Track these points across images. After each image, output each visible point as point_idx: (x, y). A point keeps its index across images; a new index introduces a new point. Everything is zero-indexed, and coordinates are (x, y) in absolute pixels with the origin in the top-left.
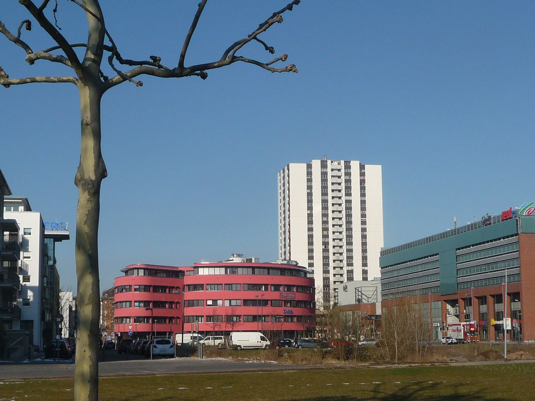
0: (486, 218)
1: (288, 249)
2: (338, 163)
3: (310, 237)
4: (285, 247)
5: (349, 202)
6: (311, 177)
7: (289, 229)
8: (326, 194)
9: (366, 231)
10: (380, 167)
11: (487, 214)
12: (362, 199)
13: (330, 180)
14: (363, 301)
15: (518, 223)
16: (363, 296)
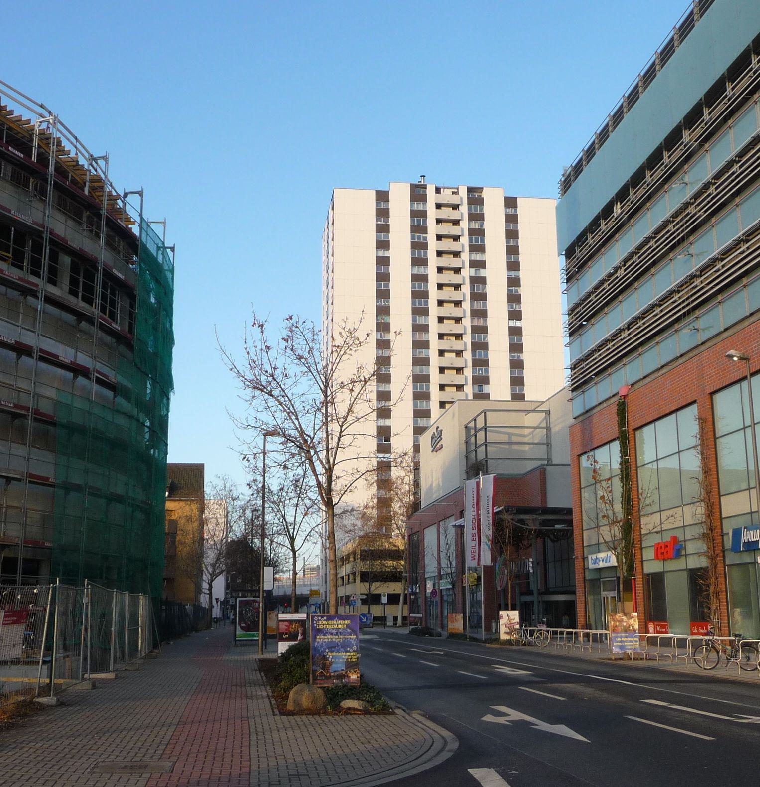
5: (478, 281)
8: (425, 312)
9: (522, 351)
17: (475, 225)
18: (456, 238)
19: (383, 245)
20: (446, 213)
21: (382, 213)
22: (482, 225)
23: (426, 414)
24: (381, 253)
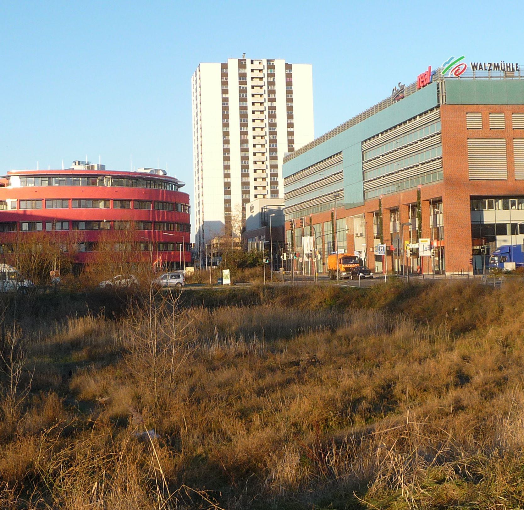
0: (398, 89)
3: (226, 151)
6: (226, 79)
10: (310, 66)
11: (399, 84)
15: (440, 89)
19: (226, 142)
21: (224, 75)
22: (274, 80)
23: (248, 201)
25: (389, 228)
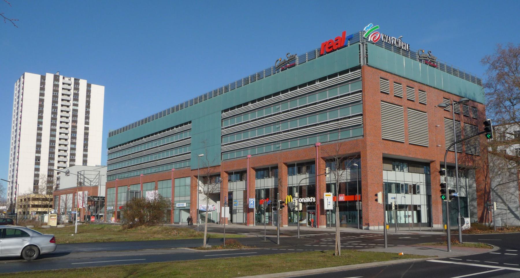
1: (18, 143)
2: (69, 79)
3: (39, 135)
4: (14, 160)
5: (75, 111)
7: (17, 174)
12: (84, 159)
13: (61, 91)
14: (86, 184)
16: (86, 180)
17: (73, 146)
18: (68, 112)
19: (40, 129)
20: (66, 86)
24: (41, 97)
25: (75, 230)
